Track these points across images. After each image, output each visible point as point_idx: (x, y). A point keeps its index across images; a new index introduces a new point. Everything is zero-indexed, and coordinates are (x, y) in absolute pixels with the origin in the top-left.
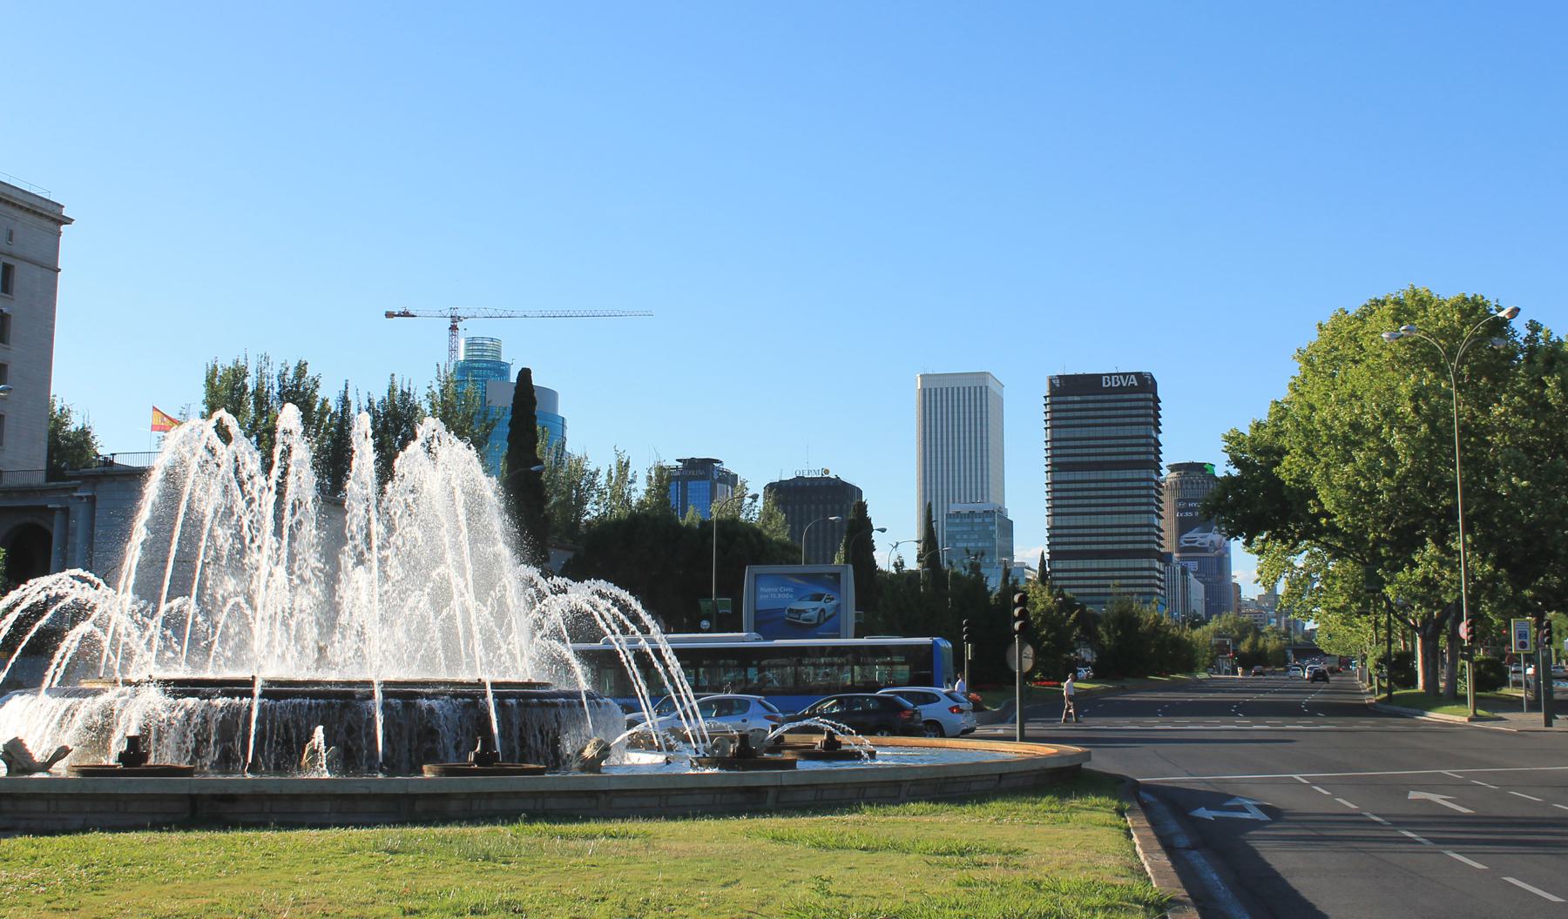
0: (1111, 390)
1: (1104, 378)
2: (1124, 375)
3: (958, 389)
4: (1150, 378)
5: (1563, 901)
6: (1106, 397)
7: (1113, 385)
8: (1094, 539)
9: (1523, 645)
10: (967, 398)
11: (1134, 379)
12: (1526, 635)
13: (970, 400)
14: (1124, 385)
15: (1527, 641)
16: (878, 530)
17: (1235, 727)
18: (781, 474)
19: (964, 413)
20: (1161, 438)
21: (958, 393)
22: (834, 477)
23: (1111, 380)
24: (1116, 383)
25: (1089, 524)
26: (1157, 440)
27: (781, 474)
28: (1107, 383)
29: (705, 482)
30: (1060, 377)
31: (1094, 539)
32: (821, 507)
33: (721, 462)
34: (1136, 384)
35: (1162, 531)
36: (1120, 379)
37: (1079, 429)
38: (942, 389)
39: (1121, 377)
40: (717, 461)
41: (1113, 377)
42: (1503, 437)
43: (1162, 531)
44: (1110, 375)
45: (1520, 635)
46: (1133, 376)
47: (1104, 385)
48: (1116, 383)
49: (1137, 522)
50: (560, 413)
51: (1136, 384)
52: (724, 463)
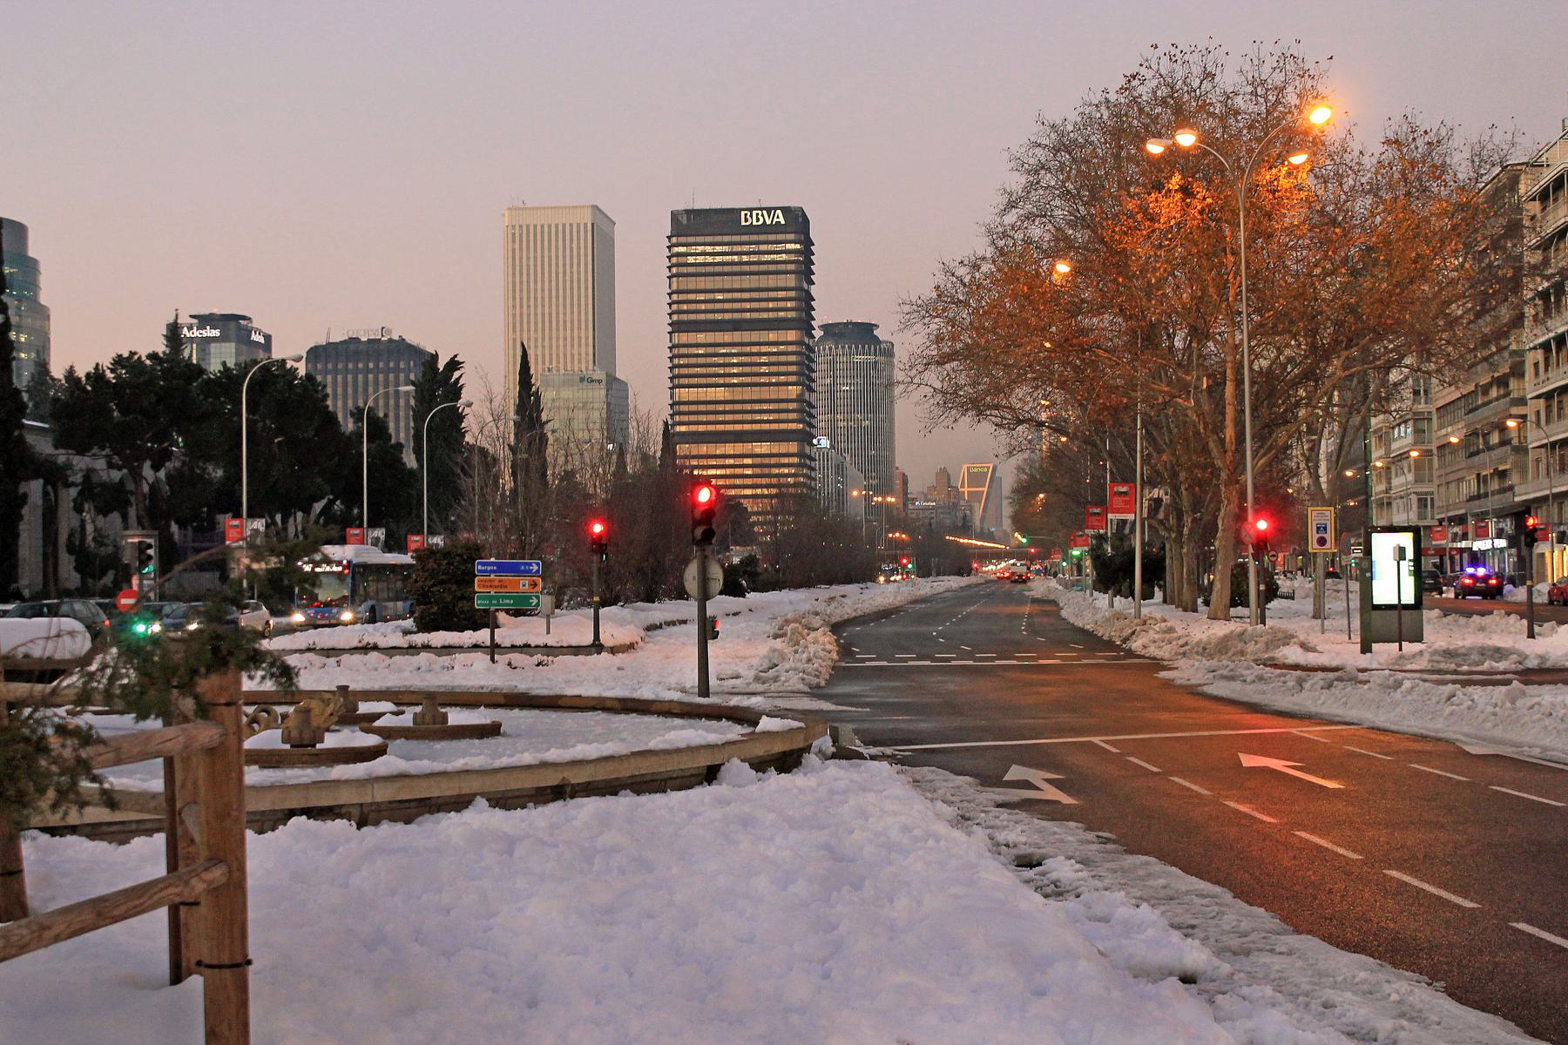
0: (752, 229)
1: (743, 213)
2: (769, 210)
3: (542, 226)
4: (800, 214)
5: (1075, 802)
6: (745, 238)
7: (755, 223)
8: (738, 417)
9: (1322, 542)
10: (568, 238)
11: (781, 215)
12: (1325, 528)
13: (571, 240)
14: (768, 222)
15: (1327, 536)
16: (1531, 399)
17: (1015, 662)
18: (328, 334)
19: (564, 257)
20: (814, 290)
21: (542, 232)
22: (397, 338)
23: (751, 216)
24: (758, 220)
25: (776, 397)
26: (808, 293)
27: (328, 334)
28: (746, 220)
29: (228, 344)
30: (688, 212)
31: (738, 417)
32: (381, 377)
33: (249, 319)
34: (783, 222)
35: (814, 407)
36: (762, 215)
37: (738, 278)
38: (535, 226)
39: (765, 212)
40: (244, 318)
41: (754, 213)
42: (1525, 275)
43: (814, 407)
44: (751, 210)
45: (1318, 528)
46: (779, 212)
47: (743, 223)
48: (758, 220)
49: (746, 397)
50: (31, 253)
51: (783, 222)
52: (254, 320)
